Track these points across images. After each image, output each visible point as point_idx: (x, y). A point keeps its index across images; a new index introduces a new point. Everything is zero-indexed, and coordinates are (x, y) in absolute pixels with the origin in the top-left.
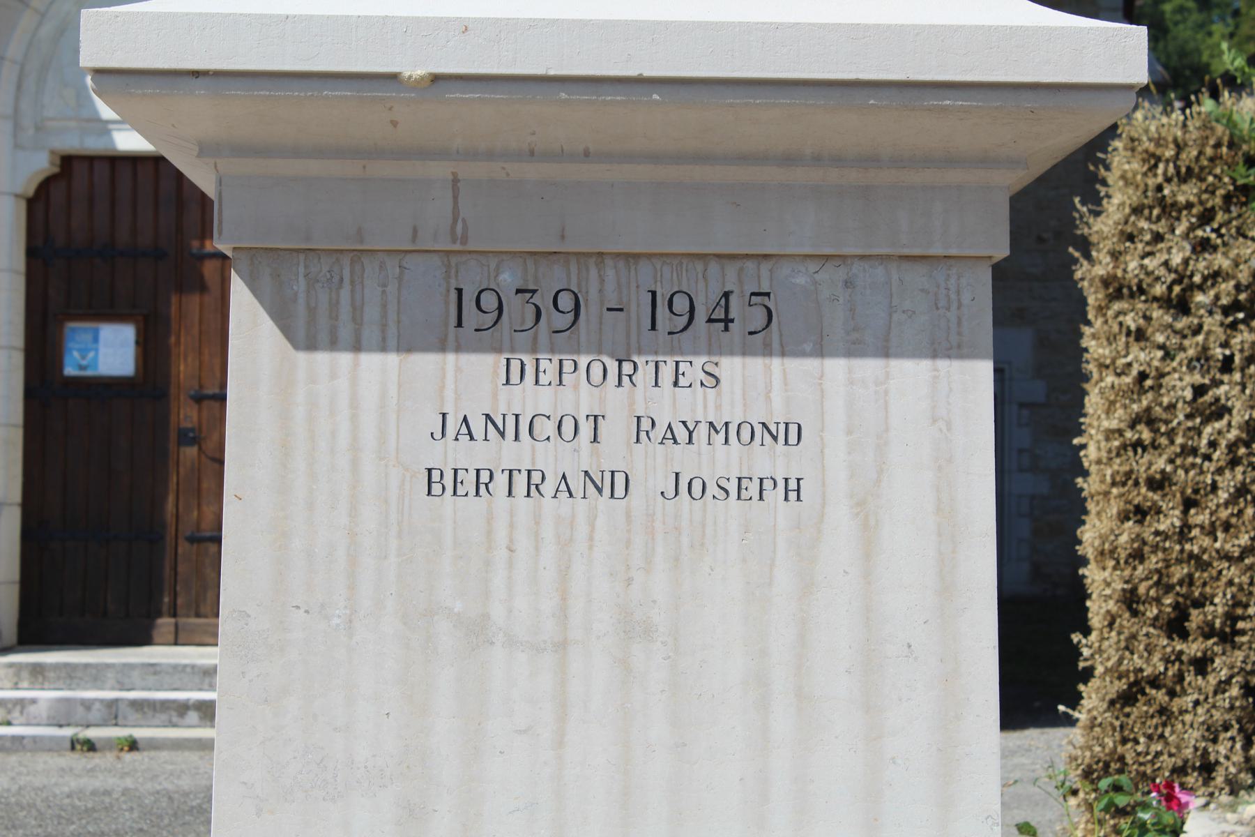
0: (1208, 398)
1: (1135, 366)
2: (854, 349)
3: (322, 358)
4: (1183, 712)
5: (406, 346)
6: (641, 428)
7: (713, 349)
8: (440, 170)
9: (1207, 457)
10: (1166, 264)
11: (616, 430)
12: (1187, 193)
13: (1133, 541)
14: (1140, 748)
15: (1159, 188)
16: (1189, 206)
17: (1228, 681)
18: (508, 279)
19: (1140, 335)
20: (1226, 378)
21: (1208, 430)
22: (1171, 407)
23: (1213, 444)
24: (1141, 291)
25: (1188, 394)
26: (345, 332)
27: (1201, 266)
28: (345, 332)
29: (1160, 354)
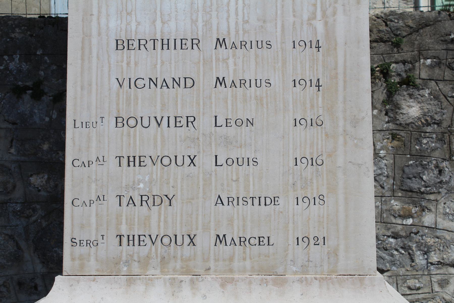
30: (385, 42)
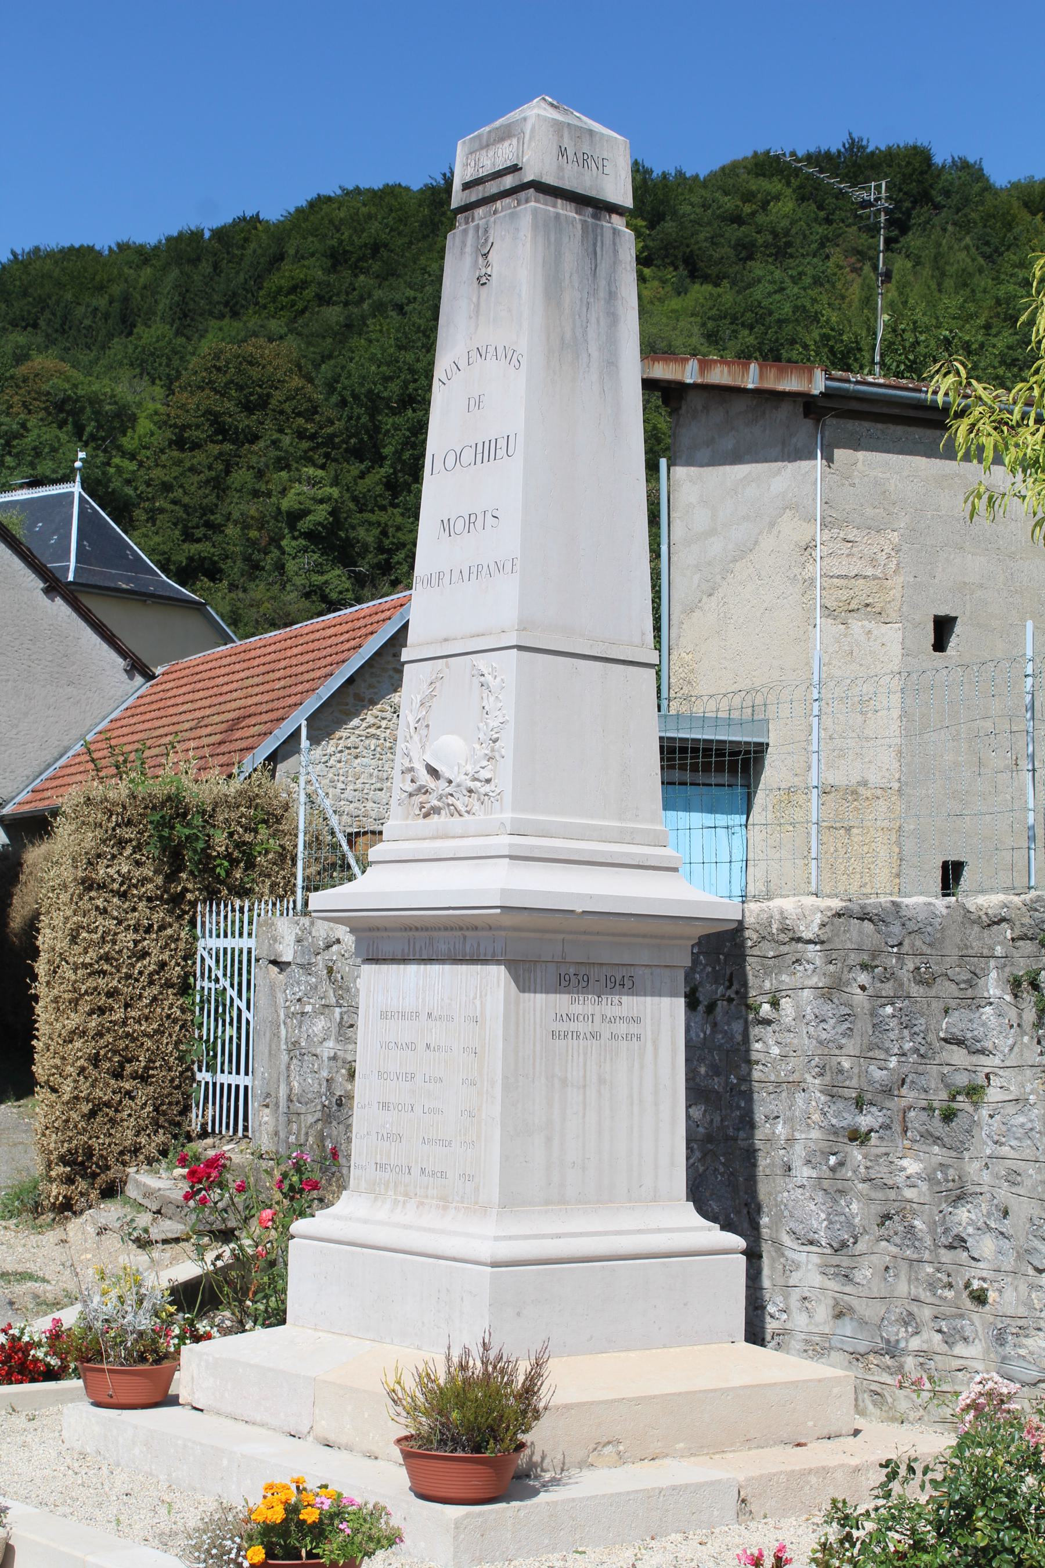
0: (139, 947)
1: (101, 927)
2: (653, 995)
3: (526, 995)
4: (122, 1120)
5: (547, 992)
6: (603, 1017)
7: (621, 994)
8: (561, 937)
9: (137, 980)
10: (118, 872)
11: (598, 1019)
12: (128, 833)
13: (98, 1025)
14: (101, 1141)
15: (114, 829)
16: (131, 840)
17: (145, 1104)
18: (572, 971)
19: (105, 911)
20: (147, 936)
21: (139, 965)
22: (120, 952)
23: (141, 973)
24: (105, 886)
25: (131, 945)
26: (532, 988)
27: (137, 873)
28: (532, 988)
29: (115, 922)
30: (1031, 939)
